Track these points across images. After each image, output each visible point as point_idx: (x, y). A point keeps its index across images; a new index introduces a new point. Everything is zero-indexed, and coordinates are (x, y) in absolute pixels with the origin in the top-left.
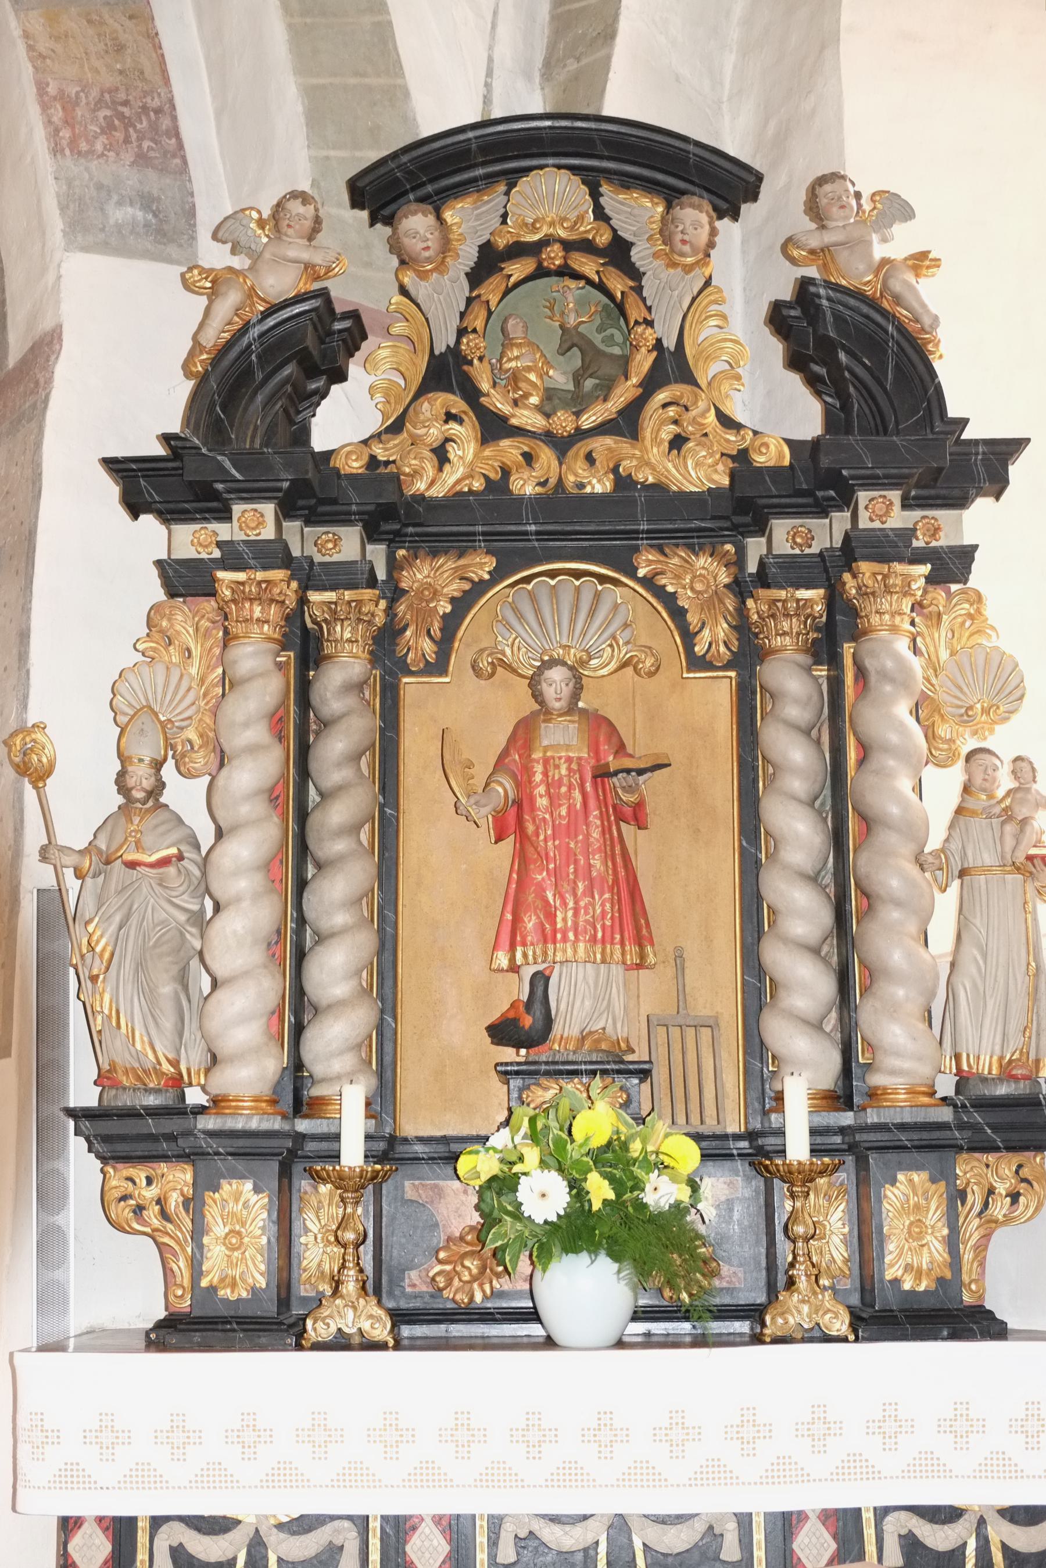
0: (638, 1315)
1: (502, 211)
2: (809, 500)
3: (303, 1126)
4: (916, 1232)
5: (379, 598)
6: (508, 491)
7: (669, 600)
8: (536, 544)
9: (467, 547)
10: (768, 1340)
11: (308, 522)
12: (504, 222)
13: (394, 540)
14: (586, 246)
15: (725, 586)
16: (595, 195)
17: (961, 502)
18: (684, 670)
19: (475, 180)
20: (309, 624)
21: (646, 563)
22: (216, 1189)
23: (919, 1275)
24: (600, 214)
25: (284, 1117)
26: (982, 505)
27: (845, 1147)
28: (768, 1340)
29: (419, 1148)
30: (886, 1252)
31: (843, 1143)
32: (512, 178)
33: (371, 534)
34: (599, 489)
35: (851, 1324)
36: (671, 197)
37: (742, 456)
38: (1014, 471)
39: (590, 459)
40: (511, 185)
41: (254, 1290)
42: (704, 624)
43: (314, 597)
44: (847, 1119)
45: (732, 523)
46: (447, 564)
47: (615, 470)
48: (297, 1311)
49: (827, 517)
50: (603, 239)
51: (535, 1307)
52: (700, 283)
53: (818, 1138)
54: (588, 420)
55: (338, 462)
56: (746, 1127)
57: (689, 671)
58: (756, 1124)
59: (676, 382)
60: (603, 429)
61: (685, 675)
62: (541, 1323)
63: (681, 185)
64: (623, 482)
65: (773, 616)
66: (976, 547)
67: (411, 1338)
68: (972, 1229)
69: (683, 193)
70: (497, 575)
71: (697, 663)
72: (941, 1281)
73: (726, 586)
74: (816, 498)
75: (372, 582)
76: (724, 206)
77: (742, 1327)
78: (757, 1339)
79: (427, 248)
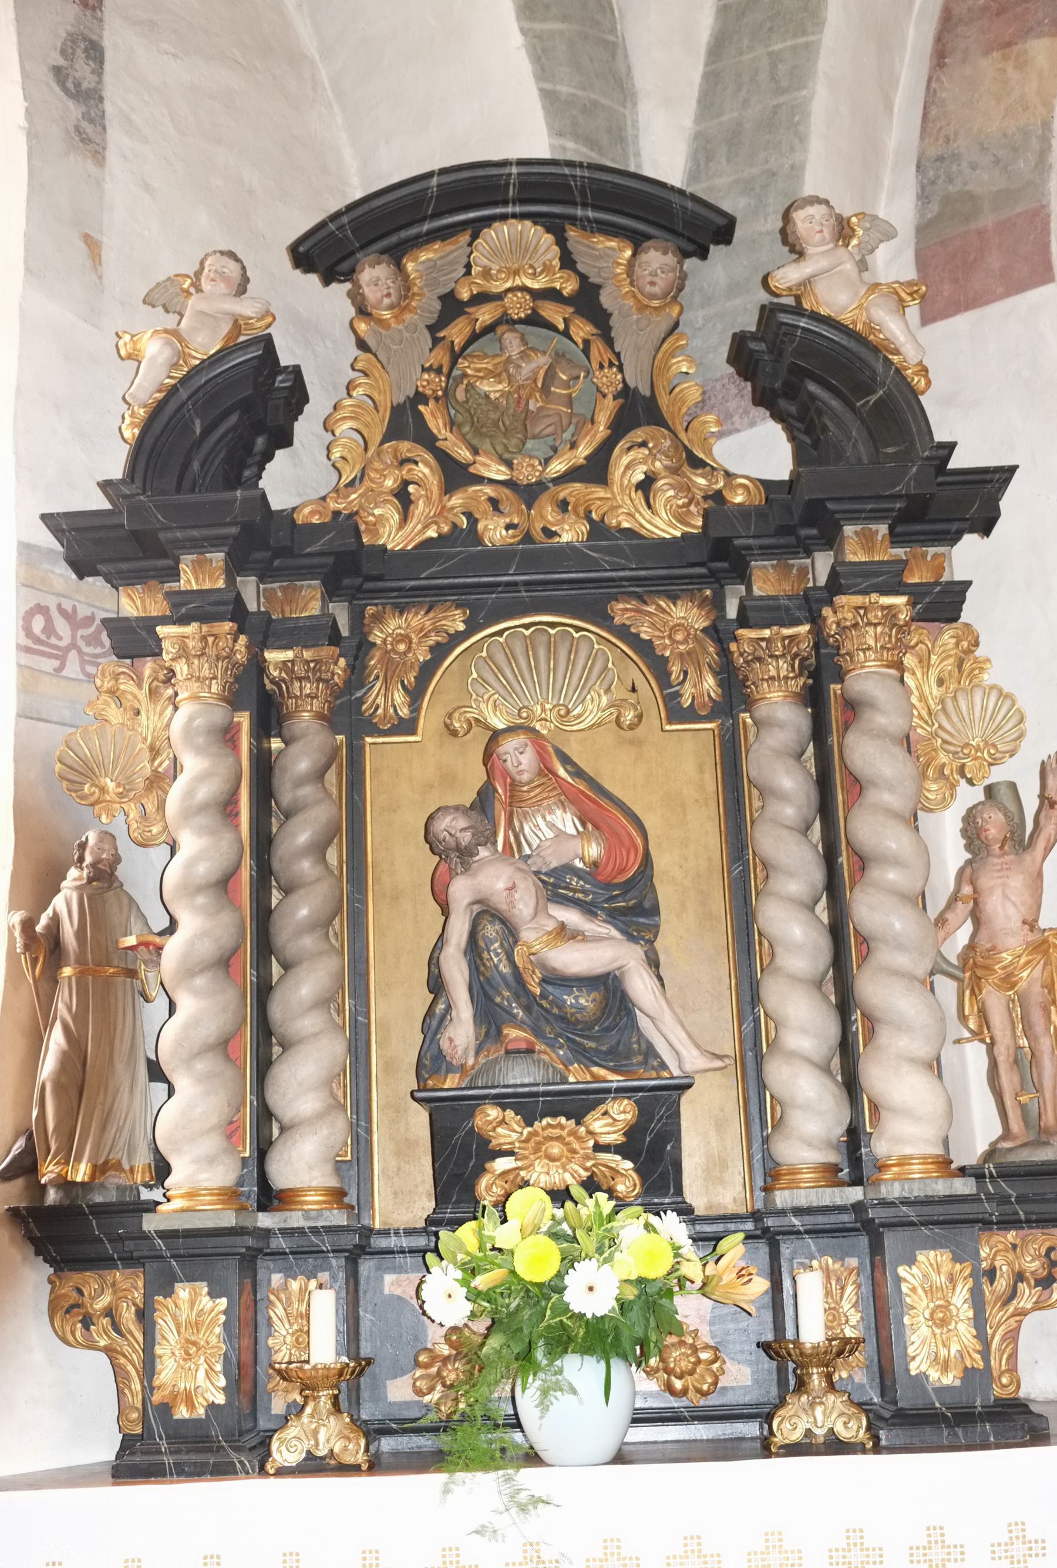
0: (640, 1418)
1: (465, 260)
2: (792, 540)
3: (265, 1220)
4: (941, 1319)
5: (340, 655)
6: (478, 540)
7: (644, 648)
8: (524, 594)
9: (407, 603)
10: (272, 1471)
11: (262, 579)
12: (468, 272)
13: (356, 597)
14: (552, 295)
15: (702, 631)
16: (561, 241)
17: (953, 539)
18: (664, 722)
19: (418, 236)
20: (269, 686)
21: (621, 611)
22: (169, 1293)
23: (945, 1368)
24: (567, 261)
25: (241, 1209)
26: (970, 541)
27: (759, 1232)
28: (272, 1471)
29: (392, 1242)
30: (908, 1343)
31: (756, 1229)
32: (477, 227)
33: (332, 592)
34: (566, 537)
35: (869, 1428)
36: (638, 241)
37: (718, 497)
38: (1006, 503)
39: (563, 506)
40: (475, 236)
41: (212, 1407)
42: (686, 673)
43: (274, 656)
44: (855, 1194)
45: (709, 569)
46: (416, 620)
47: (588, 517)
48: (263, 1424)
49: (808, 557)
50: (569, 286)
51: (516, 1414)
52: (664, 326)
53: (807, 1217)
54: (557, 467)
55: (300, 518)
56: (753, 1206)
57: (670, 723)
58: (759, 1205)
59: (649, 424)
60: (571, 475)
61: (668, 727)
62: (523, 1431)
63: (641, 227)
64: (598, 530)
65: (759, 659)
66: (968, 584)
67: (396, 1454)
68: (996, 1315)
69: (649, 237)
70: (473, 627)
71: (676, 713)
72: (969, 1373)
73: (704, 630)
74: (798, 537)
75: (335, 638)
76: (690, 247)
77: (751, 1429)
78: (766, 1448)
79: (652, 283)
